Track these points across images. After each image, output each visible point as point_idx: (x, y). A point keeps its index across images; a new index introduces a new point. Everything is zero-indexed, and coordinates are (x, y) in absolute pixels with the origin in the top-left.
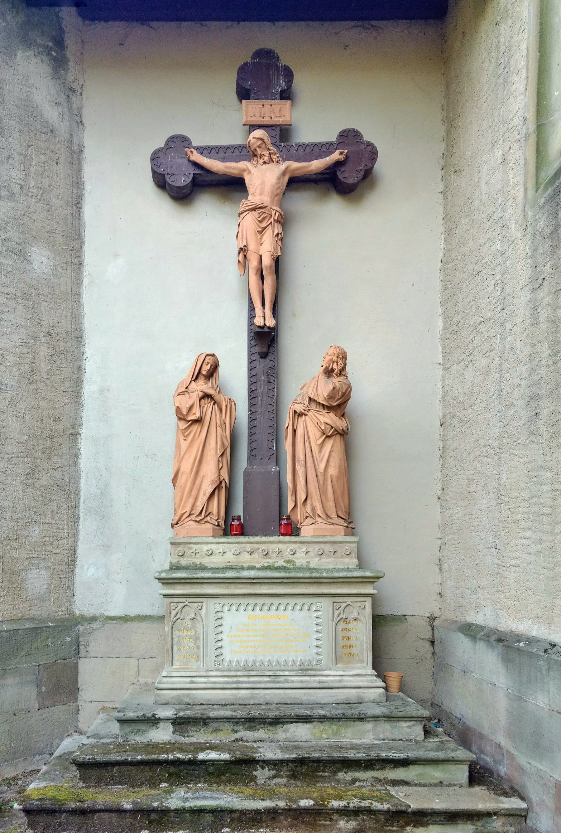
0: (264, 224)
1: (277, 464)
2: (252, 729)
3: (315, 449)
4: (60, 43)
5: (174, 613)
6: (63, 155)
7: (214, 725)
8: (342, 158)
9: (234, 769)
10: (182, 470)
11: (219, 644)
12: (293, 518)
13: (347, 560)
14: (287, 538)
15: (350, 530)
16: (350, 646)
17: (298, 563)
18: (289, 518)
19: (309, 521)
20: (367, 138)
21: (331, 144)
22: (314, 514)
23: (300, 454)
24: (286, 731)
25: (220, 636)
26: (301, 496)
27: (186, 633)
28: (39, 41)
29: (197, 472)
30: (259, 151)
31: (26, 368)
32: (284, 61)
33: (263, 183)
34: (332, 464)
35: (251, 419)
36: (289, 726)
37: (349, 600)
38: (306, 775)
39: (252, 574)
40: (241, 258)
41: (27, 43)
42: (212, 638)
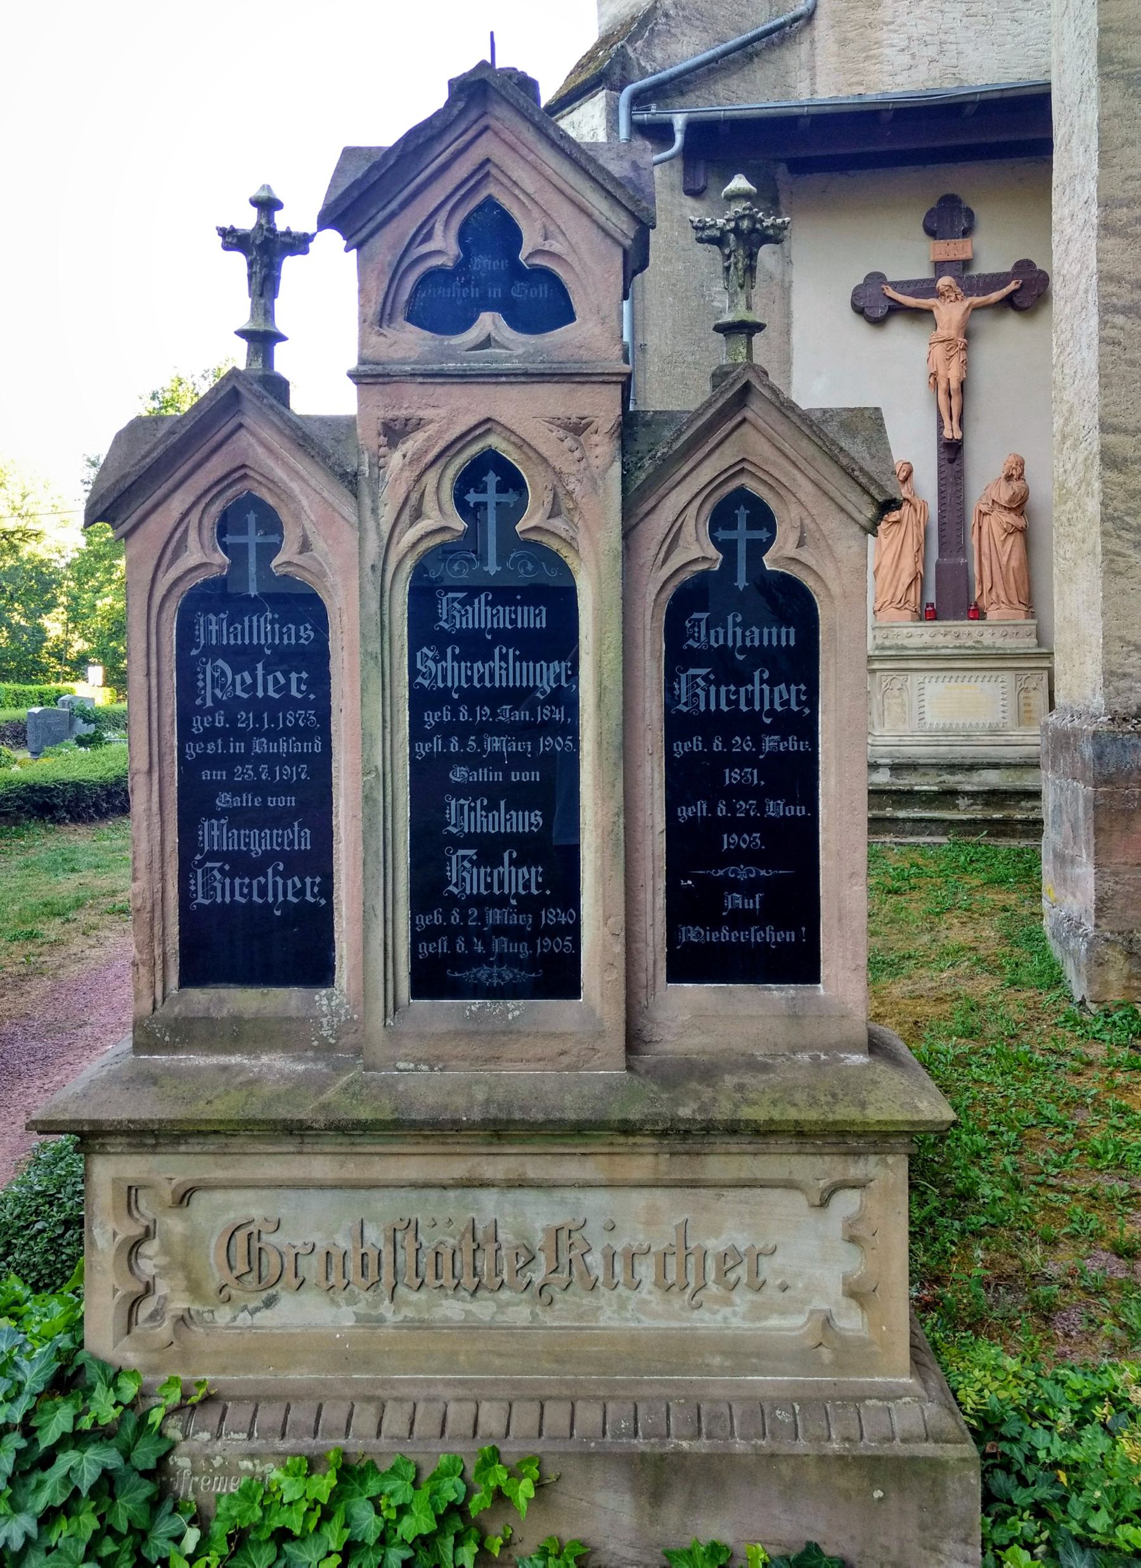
0: (952, 353)
1: (965, 557)
2: (952, 774)
3: (999, 544)
5: (884, 684)
6: (778, 293)
7: (922, 770)
8: (1017, 286)
9: (942, 798)
10: (883, 563)
11: (922, 710)
12: (979, 604)
13: (1027, 640)
14: (976, 622)
15: (1031, 613)
16: (1031, 711)
17: (985, 643)
18: (976, 605)
19: (994, 606)
21: (1007, 274)
22: (999, 601)
23: (985, 549)
24: (980, 775)
25: (922, 703)
26: (987, 585)
27: (894, 700)
29: (897, 566)
30: (947, 294)
32: (968, 203)
33: (950, 320)
34: (1013, 557)
35: (941, 516)
36: (981, 771)
37: (1029, 673)
38: (997, 803)
39: (948, 651)
40: (932, 380)
42: (916, 704)
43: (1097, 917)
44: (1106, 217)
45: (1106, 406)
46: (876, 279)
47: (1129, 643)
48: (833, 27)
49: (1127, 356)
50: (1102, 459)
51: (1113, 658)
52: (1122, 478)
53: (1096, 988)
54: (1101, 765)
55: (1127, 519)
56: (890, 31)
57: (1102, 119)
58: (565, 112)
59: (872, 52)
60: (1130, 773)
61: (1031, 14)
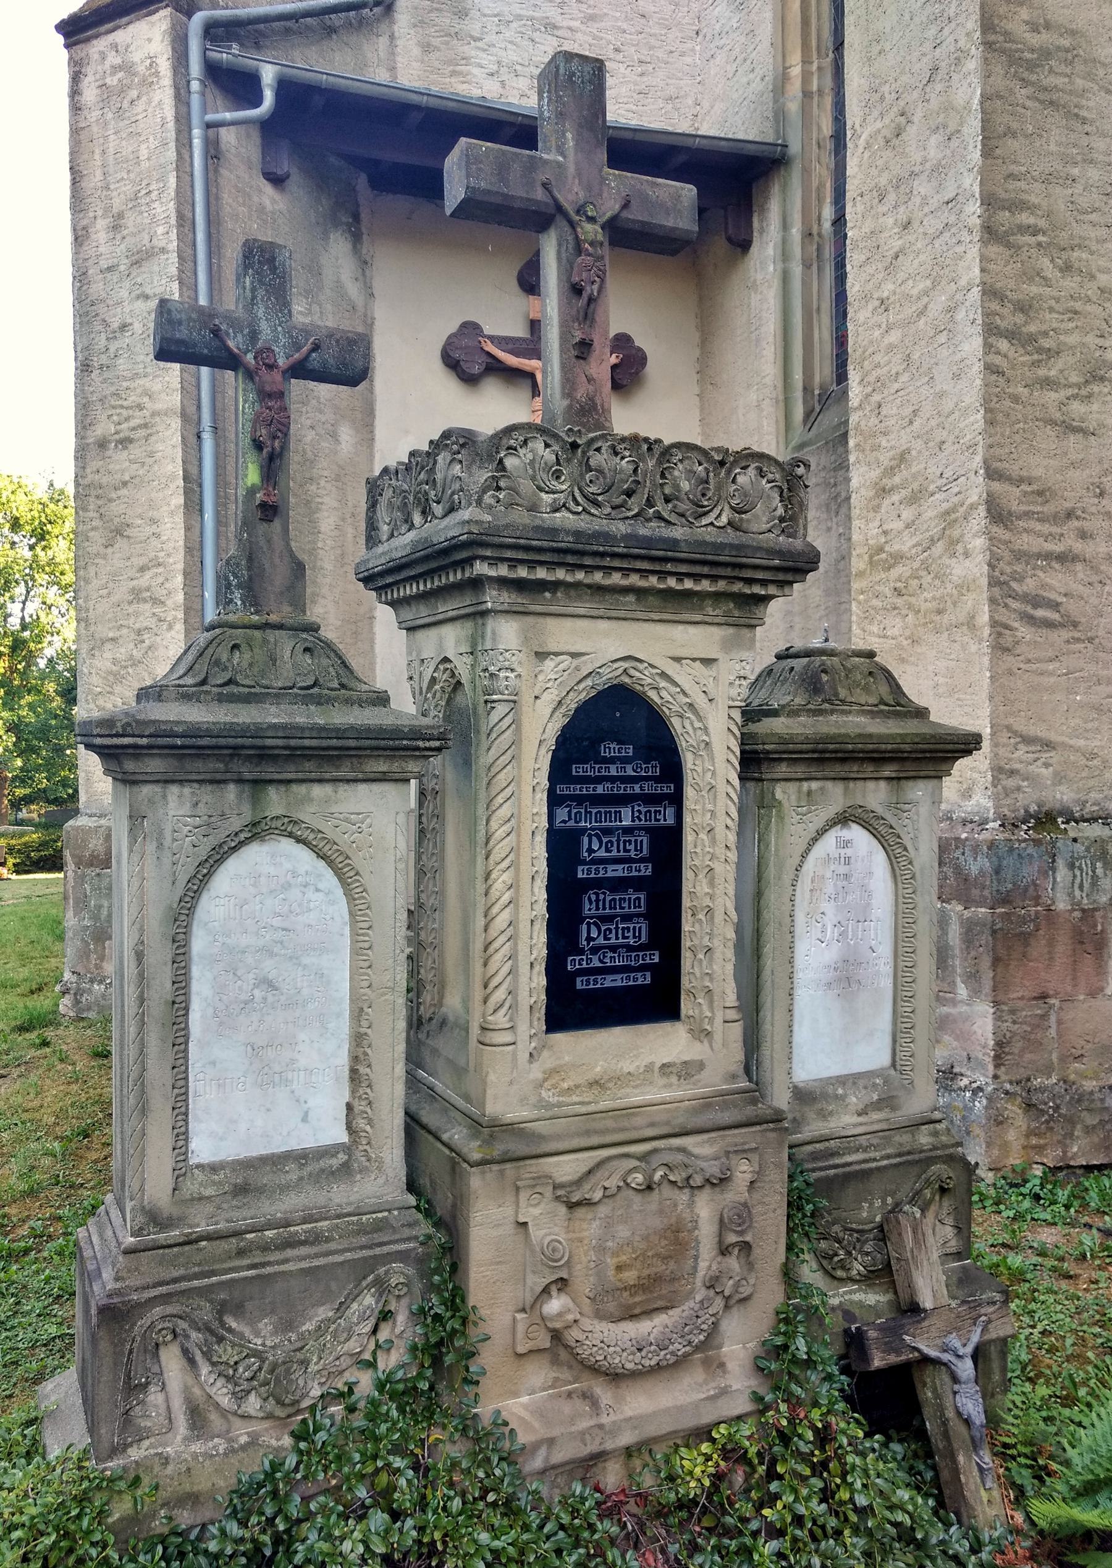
4: (356, 217)
20: (638, 342)
28: (344, 219)
31: (339, 552)
41: (336, 224)
43: (997, 1066)
44: (990, 217)
45: (991, 446)
46: (470, 329)
47: (1016, 733)
48: (415, 26)
49: (1010, 390)
50: (989, 511)
51: (1002, 751)
52: (1007, 536)
53: (996, 1152)
54: (999, 881)
55: (1014, 585)
56: (478, 48)
57: (985, 98)
58: (103, 29)
59: (459, 68)
60: (1026, 890)
61: (622, 67)
